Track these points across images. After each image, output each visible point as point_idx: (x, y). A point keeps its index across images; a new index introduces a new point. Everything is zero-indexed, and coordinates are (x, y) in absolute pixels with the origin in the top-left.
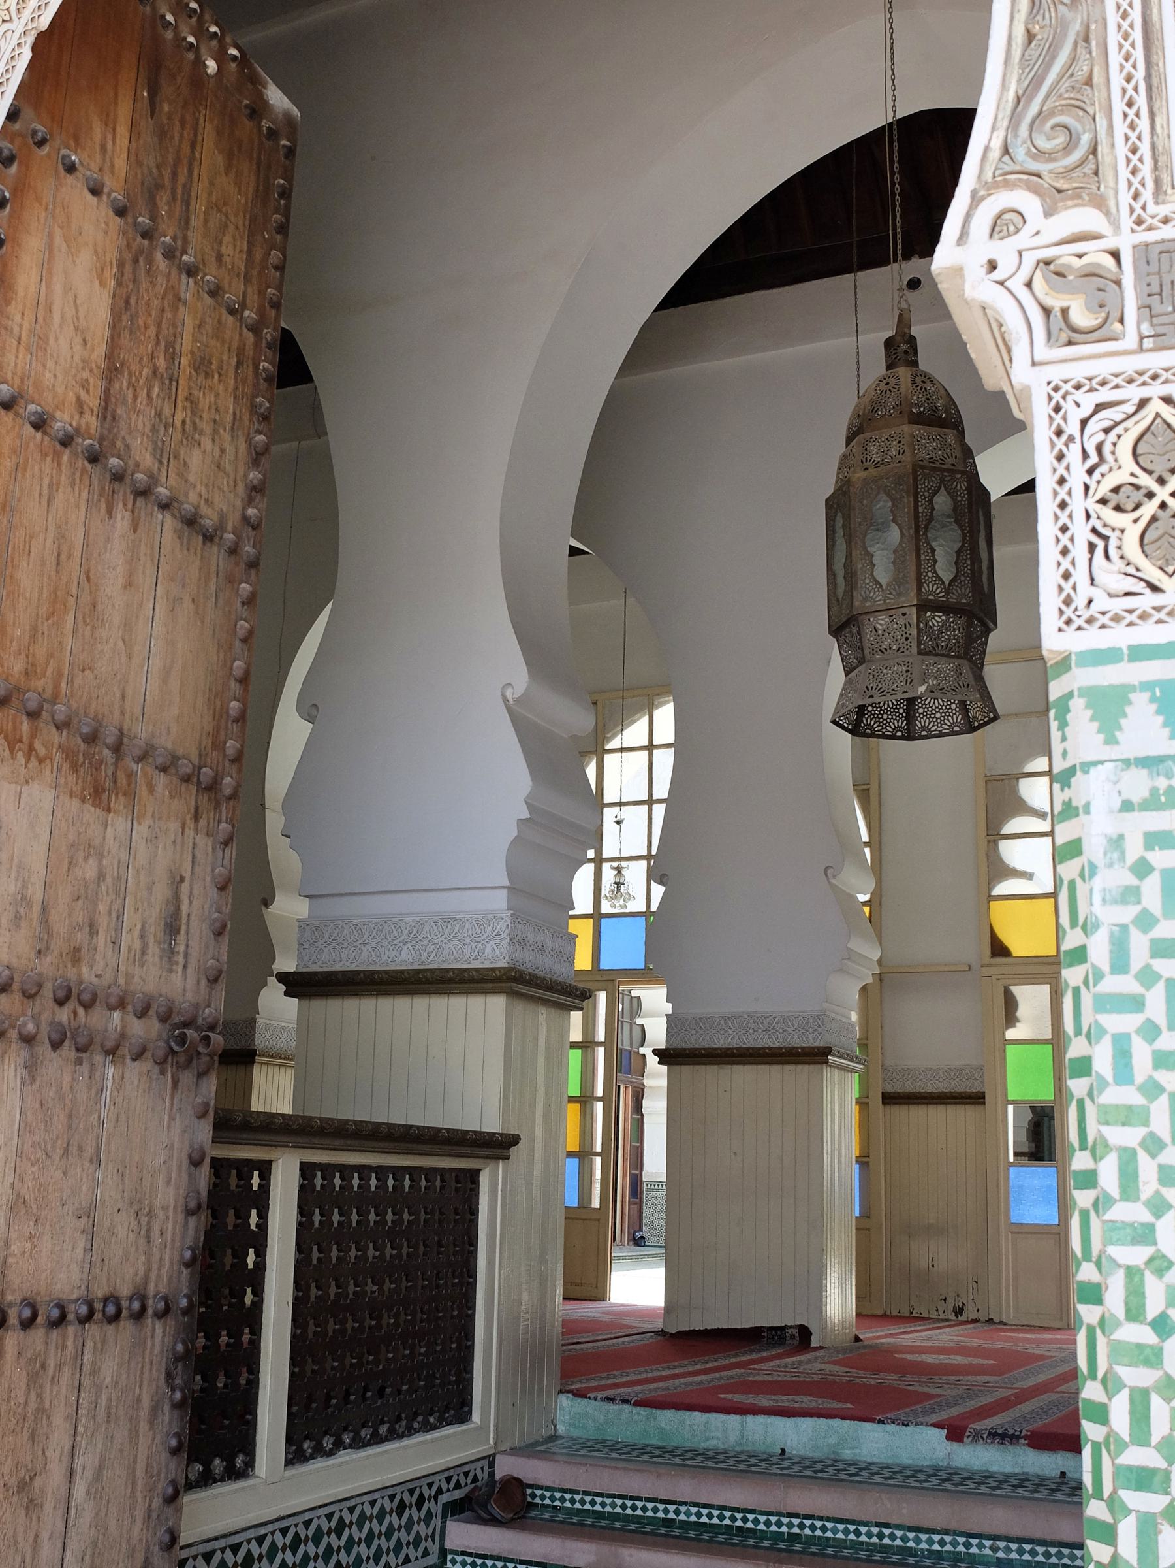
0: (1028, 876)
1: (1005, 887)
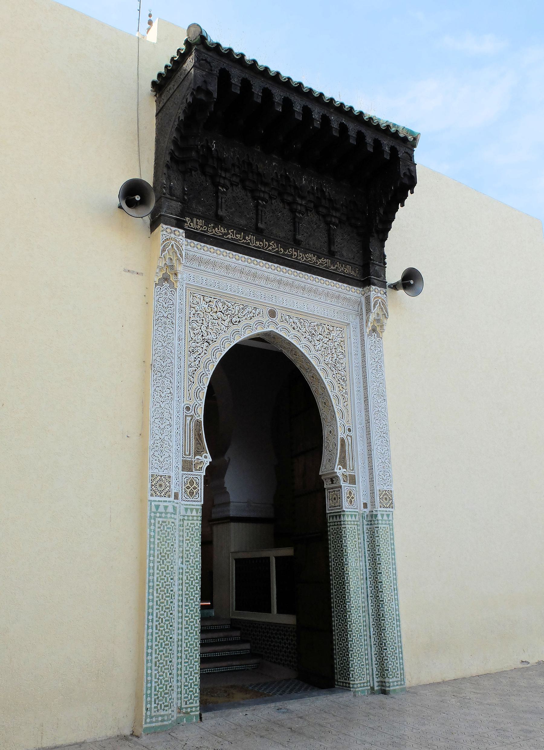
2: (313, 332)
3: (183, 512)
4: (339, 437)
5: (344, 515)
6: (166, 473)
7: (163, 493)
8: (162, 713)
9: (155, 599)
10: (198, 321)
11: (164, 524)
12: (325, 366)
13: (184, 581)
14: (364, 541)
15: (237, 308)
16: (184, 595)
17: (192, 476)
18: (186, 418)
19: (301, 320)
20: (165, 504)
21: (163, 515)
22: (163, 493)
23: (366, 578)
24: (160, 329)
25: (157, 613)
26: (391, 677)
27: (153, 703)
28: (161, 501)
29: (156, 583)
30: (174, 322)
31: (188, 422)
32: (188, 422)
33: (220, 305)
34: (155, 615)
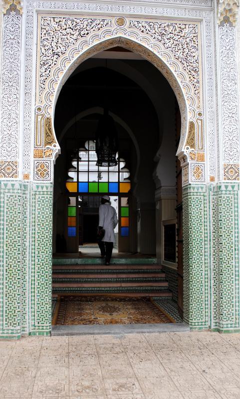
0: (73, 178)
1: (68, 181)
2: (164, 32)
3: (35, 189)
4: (188, 121)
5: (190, 188)
6: (13, 159)
7: (11, 175)
8: (12, 328)
9: (5, 251)
10: (49, 39)
11: (12, 197)
12: (176, 61)
13: (36, 238)
14: (209, 209)
15: (86, 23)
16: (36, 249)
17: (42, 162)
18: (37, 117)
19: (151, 24)
20: (13, 183)
21: (11, 191)
22: (11, 175)
23: (210, 240)
24: (7, 49)
25: (7, 261)
26: (225, 320)
27: (4, 321)
28: (9, 181)
29: (5, 240)
30: (20, 41)
31: (39, 120)
32: (39, 120)
33: (69, 22)
34: (5, 262)
